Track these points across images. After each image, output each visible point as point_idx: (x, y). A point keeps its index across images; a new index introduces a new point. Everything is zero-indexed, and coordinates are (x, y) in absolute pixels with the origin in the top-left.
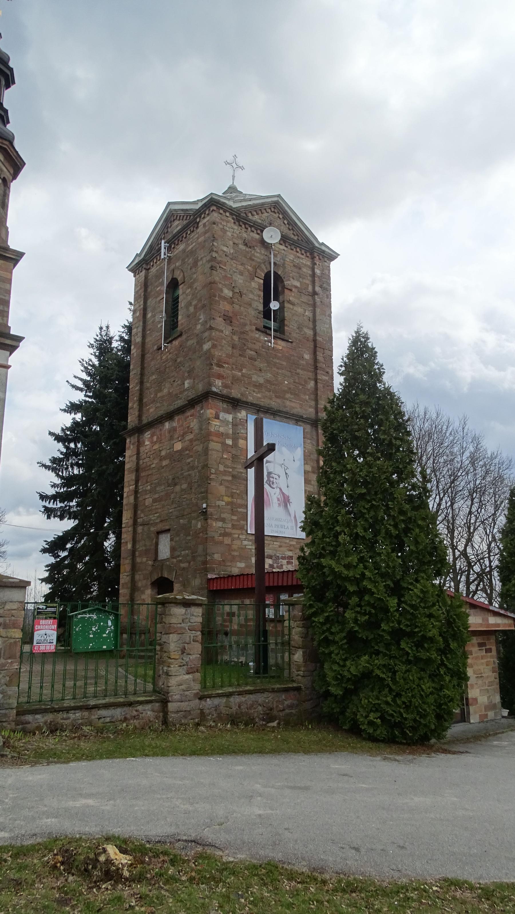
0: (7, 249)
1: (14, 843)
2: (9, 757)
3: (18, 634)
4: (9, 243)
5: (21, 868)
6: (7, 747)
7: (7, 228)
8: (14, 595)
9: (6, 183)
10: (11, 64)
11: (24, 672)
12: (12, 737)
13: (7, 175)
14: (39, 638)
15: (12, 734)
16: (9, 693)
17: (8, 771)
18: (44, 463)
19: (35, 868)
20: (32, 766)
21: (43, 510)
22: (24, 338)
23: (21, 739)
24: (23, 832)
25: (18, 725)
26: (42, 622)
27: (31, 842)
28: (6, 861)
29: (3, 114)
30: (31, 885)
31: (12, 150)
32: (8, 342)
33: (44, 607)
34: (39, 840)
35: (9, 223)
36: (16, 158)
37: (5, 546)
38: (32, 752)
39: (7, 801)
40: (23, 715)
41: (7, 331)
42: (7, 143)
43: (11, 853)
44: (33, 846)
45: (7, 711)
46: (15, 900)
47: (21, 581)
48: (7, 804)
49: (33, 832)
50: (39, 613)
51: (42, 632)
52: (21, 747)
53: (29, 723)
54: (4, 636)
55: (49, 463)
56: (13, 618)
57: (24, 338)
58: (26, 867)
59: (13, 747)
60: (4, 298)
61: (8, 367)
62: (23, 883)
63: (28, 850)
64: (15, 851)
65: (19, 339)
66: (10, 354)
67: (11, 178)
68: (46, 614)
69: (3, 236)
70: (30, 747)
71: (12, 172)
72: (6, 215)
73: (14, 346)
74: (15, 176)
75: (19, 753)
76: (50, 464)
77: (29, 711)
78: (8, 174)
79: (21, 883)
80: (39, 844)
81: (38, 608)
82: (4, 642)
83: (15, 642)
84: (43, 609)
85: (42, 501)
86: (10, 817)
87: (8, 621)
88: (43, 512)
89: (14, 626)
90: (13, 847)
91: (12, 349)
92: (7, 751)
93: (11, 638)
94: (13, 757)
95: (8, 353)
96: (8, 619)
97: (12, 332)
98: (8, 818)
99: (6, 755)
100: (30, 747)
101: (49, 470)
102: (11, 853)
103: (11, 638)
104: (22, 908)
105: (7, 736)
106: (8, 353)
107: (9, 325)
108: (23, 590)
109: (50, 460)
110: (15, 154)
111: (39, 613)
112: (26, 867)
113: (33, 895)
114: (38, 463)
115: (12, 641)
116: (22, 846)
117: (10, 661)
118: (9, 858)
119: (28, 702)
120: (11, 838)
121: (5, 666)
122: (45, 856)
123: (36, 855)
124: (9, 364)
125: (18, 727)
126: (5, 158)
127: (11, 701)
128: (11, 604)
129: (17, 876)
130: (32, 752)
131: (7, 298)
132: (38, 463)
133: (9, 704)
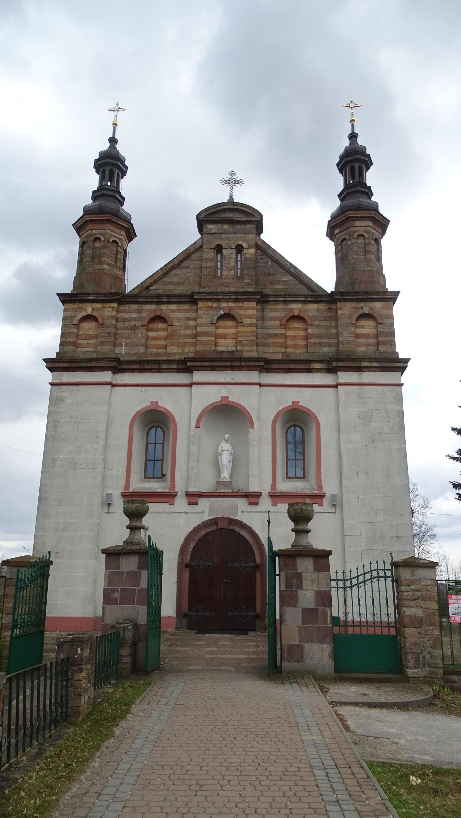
0: (386, 292)
1: (434, 764)
2: (439, 706)
3: (435, 606)
4: (387, 287)
5: (438, 782)
6: (437, 698)
7: (383, 276)
8: (421, 573)
9: (378, 242)
10: (368, 152)
11: (456, 641)
12: (441, 691)
13: (377, 235)
14: (454, 610)
15: (442, 689)
16: (435, 654)
17: (437, 716)
18: (451, 455)
19: (448, 784)
20: (458, 717)
21: (457, 497)
22: (410, 359)
23: (450, 695)
24: (443, 759)
25: (447, 683)
26: (454, 597)
27: (448, 767)
28: (428, 775)
29: (367, 191)
30: (445, 795)
31: (378, 215)
32: (398, 365)
33: (454, 584)
34: (454, 767)
35: (385, 271)
36: (381, 219)
37: (435, 529)
38: (458, 706)
39: (433, 736)
40: (449, 674)
41: (396, 357)
42: (373, 212)
43: (431, 770)
44: (449, 770)
45: (435, 670)
46: (432, 801)
47: (431, 562)
48: (433, 738)
49: (451, 761)
50: (450, 589)
51: (456, 605)
52: (449, 700)
53: (456, 682)
54: (424, 607)
55: (456, 455)
56: (428, 592)
57: (410, 359)
58: (442, 782)
59: (443, 699)
60: (389, 330)
61: (402, 385)
62: (439, 792)
63: (444, 772)
64: (434, 770)
65: (407, 360)
66: (402, 375)
67: (381, 236)
68: (456, 591)
69: (382, 283)
70: (457, 702)
71: (380, 231)
72: (381, 265)
73: (404, 367)
74: (383, 233)
75: (447, 705)
76: (458, 456)
77: (453, 672)
78: (378, 234)
79: (438, 792)
80: (454, 770)
81: (449, 585)
82: (424, 612)
83: (433, 613)
84: (453, 586)
85: (456, 489)
86: (434, 747)
87: (424, 595)
88: (458, 499)
89: (431, 599)
90: (433, 767)
91: (402, 370)
92: (437, 702)
93: (429, 609)
94: (442, 707)
95: (400, 373)
96: (424, 593)
97: (400, 356)
98: (433, 748)
99: (437, 705)
100: (457, 702)
101: (457, 461)
102: (431, 770)
103: (429, 609)
104: (437, 807)
105: (437, 690)
106: (400, 373)
107: (397, 351)
108: (432, 570)
109: (457, 452)
110: (381, 217)
111: (450, 589)
112: (442, 782)
113: (446, 801)
114: (447, 456)
115: (431, 611)
116: (441, 768)
117: (431, 628)
118: (430, 774)
119: (452, 665)
120: (433, 761)
121: (428, 631)
122: (457, 779)
123: (452, 777)
124: (402, 382)
125: (446, 684)
126: (374, 223)
127: (437, 661)
128: (425, 580)
129: (434, 786)
130: (458, 706)
131: (392, 330)
132: (447, 456)
133: (436, 664)
